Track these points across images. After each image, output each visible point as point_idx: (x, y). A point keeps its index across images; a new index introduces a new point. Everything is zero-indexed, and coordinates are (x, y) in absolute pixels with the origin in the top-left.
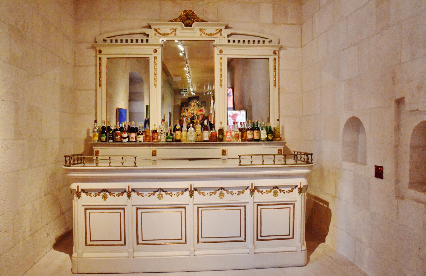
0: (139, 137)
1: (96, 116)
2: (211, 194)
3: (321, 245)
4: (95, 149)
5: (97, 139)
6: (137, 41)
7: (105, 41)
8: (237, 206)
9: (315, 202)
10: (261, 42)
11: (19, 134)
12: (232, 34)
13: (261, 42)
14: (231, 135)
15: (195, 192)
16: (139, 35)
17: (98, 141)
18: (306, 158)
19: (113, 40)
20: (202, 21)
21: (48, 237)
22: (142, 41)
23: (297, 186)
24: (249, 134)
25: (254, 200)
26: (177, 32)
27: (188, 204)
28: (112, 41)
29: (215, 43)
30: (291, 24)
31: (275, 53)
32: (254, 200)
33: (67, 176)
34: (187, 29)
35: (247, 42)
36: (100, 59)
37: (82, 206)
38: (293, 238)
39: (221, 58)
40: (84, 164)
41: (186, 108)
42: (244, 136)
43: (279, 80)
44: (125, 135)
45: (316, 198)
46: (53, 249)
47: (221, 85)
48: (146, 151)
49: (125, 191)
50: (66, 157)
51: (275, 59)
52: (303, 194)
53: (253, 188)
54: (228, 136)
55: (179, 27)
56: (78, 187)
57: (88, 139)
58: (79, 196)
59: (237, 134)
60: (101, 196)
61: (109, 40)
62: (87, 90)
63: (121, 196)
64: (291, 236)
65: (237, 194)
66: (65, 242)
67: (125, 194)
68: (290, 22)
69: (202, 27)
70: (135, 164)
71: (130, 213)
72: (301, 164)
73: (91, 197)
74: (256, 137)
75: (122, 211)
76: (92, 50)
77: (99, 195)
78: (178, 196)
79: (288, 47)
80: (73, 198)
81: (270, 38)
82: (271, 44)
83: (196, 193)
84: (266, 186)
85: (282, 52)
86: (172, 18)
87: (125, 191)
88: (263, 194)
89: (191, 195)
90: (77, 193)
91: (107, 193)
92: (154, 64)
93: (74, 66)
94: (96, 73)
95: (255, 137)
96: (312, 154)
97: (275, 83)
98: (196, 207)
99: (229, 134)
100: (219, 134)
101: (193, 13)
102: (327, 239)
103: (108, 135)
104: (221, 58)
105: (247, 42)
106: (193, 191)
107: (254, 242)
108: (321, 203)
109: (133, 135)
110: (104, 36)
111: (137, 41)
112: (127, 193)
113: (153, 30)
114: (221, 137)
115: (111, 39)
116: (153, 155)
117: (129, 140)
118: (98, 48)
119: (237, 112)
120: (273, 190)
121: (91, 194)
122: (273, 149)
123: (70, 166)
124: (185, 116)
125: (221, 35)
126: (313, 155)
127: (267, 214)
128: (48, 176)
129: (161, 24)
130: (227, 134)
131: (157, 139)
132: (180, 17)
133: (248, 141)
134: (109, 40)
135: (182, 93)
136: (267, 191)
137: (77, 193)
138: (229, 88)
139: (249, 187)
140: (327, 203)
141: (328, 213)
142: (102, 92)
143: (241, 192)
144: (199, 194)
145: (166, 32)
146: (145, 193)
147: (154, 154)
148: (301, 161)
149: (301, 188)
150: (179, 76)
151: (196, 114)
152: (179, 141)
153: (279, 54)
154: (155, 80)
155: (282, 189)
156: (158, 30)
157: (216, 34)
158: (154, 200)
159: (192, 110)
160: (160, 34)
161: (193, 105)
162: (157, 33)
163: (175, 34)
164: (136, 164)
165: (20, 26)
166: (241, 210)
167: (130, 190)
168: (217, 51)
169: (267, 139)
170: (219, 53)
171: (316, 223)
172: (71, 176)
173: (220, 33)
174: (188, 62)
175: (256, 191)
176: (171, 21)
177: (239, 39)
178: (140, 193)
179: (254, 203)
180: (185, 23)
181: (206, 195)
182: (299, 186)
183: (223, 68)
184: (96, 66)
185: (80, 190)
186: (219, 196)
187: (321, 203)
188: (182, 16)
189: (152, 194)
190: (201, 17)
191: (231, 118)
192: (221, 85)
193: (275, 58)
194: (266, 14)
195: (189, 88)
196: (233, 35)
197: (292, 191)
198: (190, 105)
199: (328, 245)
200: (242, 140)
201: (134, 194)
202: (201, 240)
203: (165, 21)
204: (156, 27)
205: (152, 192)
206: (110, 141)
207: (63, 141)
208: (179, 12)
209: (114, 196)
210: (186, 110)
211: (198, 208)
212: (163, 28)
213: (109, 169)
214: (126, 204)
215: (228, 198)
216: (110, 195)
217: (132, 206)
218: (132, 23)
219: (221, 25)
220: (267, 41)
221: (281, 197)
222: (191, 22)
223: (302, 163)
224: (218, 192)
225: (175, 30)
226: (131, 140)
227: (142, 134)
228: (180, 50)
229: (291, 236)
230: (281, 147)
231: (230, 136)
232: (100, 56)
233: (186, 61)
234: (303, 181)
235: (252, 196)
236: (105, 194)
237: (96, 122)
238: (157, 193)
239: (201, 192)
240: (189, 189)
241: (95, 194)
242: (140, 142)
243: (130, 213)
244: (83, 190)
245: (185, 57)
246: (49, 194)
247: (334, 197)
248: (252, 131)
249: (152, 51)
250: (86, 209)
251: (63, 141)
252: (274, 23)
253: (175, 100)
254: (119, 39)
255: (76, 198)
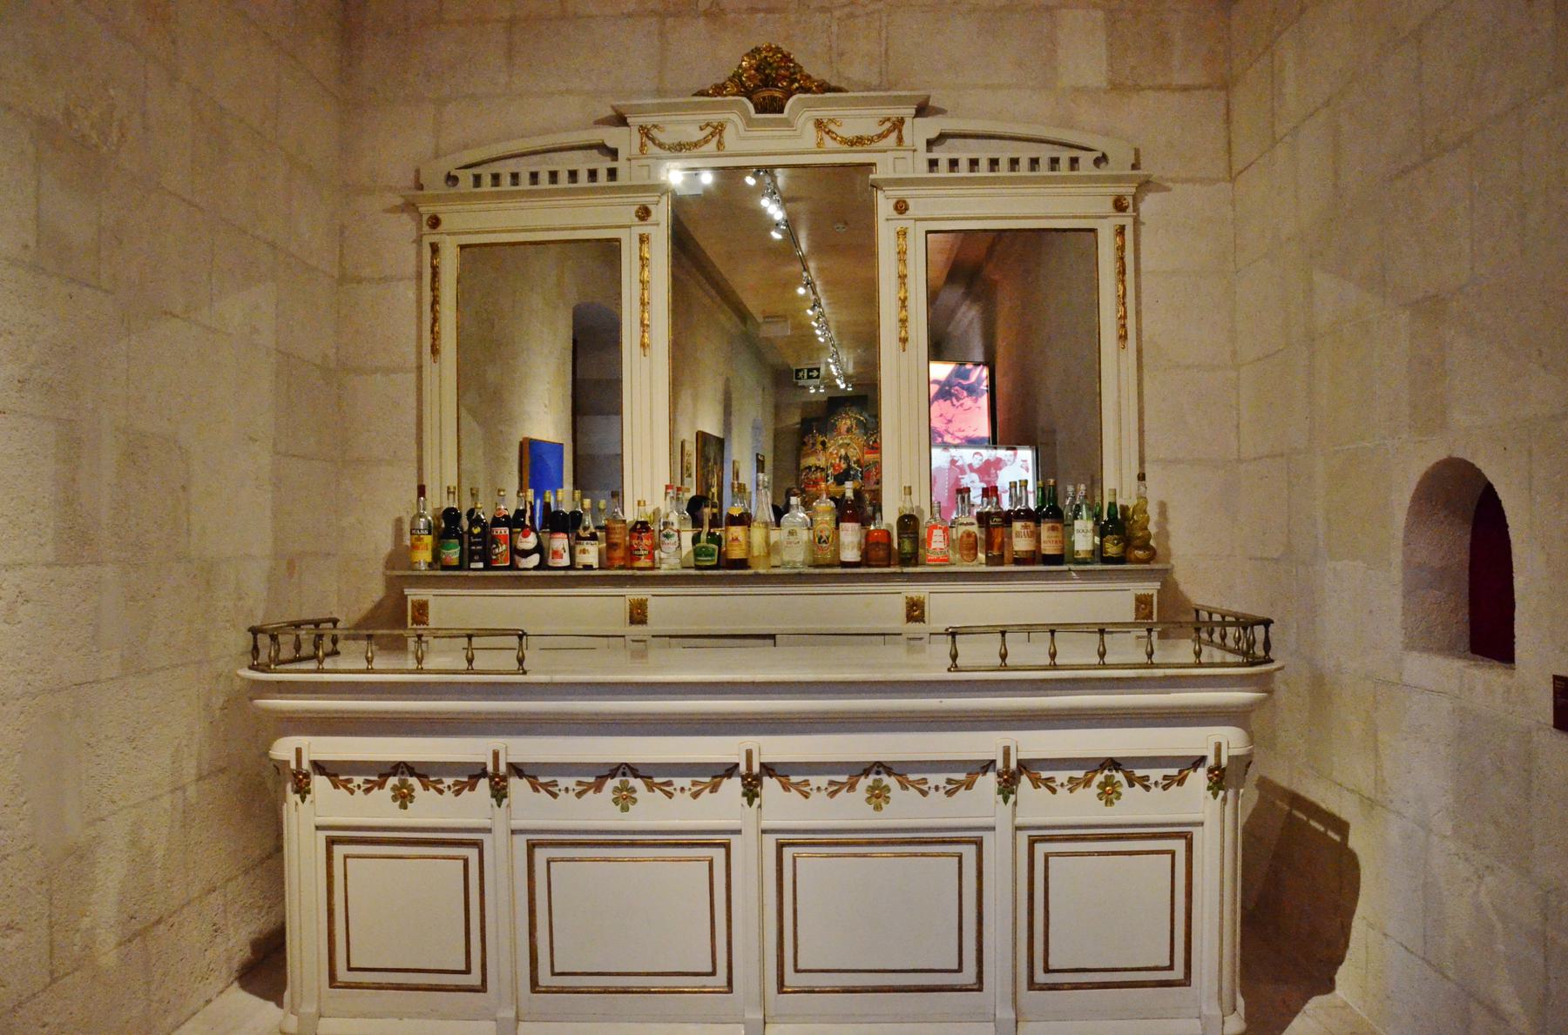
0: (584, 551)
1: (420, 469)
2: (834, 790)
3: (1315, 1002)
4: (414, 594)
5: (424, 556)
6: (573, 175)
7: (452, 179)
8: (943, 842)
9: (1290, 814)
10: (1064, 163)
11: (76, 541)
12: (943, 137)
13: (1064, 163)
14: (949, 541)
15: (766, 780)
16: (579, 153)
17: (430, 565)
18: (1250, 639)
19: (483, 178)
20: (825, 88)
21: (218, 940)
22: (593, 175)
23: (1203, 759)
24: (1018, 535)
25: (1014, 815)
26: (729, 134)
27: (738, 832)
28: (477, 180)
29: (878, 175)
30: (1185, 89)
31: (1119, 205)
32: (1014, 815)
33: (257, 708)
34: (766, 123)
35: (1004, 164)
36: (435, 249)
37: (318, 828)
38: (1186, 981)
39: (903, 234)
40: (321, 662)
41: (821, 439)
42: (999, 541)
43: (1138, 313)
44: (530, 542)
45: (1296, 800)
46: (236, 984)
47: (904, 340)
48: (605, 607)
49: (484, 774)
50: (255, 631)
51: (1121, 231)
52: (1231, 793)
53: (1013, 765)
54: (934, 546)
55: (736, 115)
56: (299, 751)
57: (399, 558)
58: (303, 790)
59: (969, 535)
60: (387, 792)
61: (466, 178)
62: (387, 371)
63: (466, 791)
64: (1178, 973)
65: (942, 791)
66: (265, 968)
67: (484, 784)
68: (1179, 79)
69: (824, 113)
70: (521, 661)
71: (504, 861)
72: (1224, 665)
73: (352, 792)
74: (1049, 548)
75: (472, 854)
76: (405, 217)
77: (381, 785)
78: (695, 795)
79: (1172, 180)
80: (284, 799)
81: (1101, 145)
82: (1104, 171)
83: (770, 785)
84: (1052, 760)
85: (1150, 204)
86: (708, 85)
87: (484, 774)
88: (1053, 791)
89: (751, 791)
90: (295, 776)
91: (413, 781)
92: (637, 263)
93: (343, 279)
94: (419, 301)
95: (1043, 546)
96: (1267, 623)
97: (1124, 326)
98: (770, 842)
99: (938, 534)
100: (899, 537)
101: (787, 58)
102: (1342, 975)
103: (468, 544)
104: (903, 234)
105: (1004, 164)
106: (758, 779)
107: (1015, 993)
108: (1313, 823)
109: (560, 542)
110: (448, 164)
111: (573, 175)
112: (491, 779)
113: (635, 130)
114: (907, 547)
115: (476, 171)
116: (632, 622)
117: (542, 565)
118: (426, 210)
119: (1002, 453)
120: (1099, 778)
121: (349, 781)
122: (1114, 599)
123: (265, 669)
124: (818, 468)
125: (900, 140)
126: (1272, 628)
127: (1074, 879)
128: (218, 701)
129: (662, 109)
130: (930, 535)
131: (651, 556)
132: (737, 76)
133: (1017, 562)
134: (466, 178)
135: (801, 383)
136: (1071, 780)
137: (295, 776)
138: (977, 364)
139: (993, 762)
140: (1342, 827)
141: (1348, 866)
142: (444, 374)
143: (960, 784)
144: (786, 787)
145: (684, 140)
146: (564, 782)
147: (638, 615)
148: (1223, 647)
149: (1218, 766)
150: (784, 318)
151: (858, 462)
152: (742, 564)
153: (1136, 209)
154: (642, 324)
155: (1139, 773)
156: (654, 132)
157: (882, 136)
158: (599, 811)
159: (841, 446)
160: (661, 145)
161: (844, 429)
162: (649, 143)
163: (720, 144)
164: (526, 665)
165: (87, 123)
166: (960, 857)
167: (503, 769)
168: (884, 205)
169: (1099, 555)
170: (895, 214)
171: (1293, 901)
172: (282, 712)
173: (894, 135)
174: (812, 265)
175: (1024, 779)
176: (702, 93)
177: (974, 156)
178: (542, 780)
179: (1018, 828)
180: (755, 97)
181: (814, 794)
182: (1211, 761)
183: (910, 272)
184: (419, 276)
185: (306, 766)
186: (868, 800)
187: (1313, 823)
188: (745, 70)
189: (589, 786)
190: (816, 70)
191: (975, 477)
192: (904, 340)
193: (1123, 228)
194: (1084, 57)
195: (828, 364)
196: (949, 142)
197: (1181, 782)
198: (834, 428)
199: (1346, 1006)
200: (990, 561)
201: (517, 786)
202: (791, 979)
203: (679, 93)
204: (648, 120)
205: (591, 780)
206: (473, 565)
207: (291, 565)
208: (731, 55)
209: (441, 792)
210: (819, 447)
211: (780, 846)
212: (671, 122)
213: (413, 684)
214: (485, 823)
215: (906, 809)
216: (426, 788)
217: (513, 832)
218: (555, 110)
219: (899, 101)
220: (1086, 159)
221: (1135, 806)
222: (778, 94)
223: (1230, 658)
224: (865, 783)
225: (718, 130)
226: (551, 563)
227: (593, 537)
228: (770, 218)
229: (1178, 973)
230: (1151, 588)
231: (942, 546)
232: (435, 239)
233: (803, 261)
234: (1231, 740)
235: (1006, 800)
236: (403, 784)
237: (421, 491)
238: (611, 784)
239: (794, 779)
240: (743, 769)
241: (367, 781)
242: (589, 567)
243: (504, 861)
244: (319, 767)
245: (797, 244)
246: (222, 770)
247: (1370, 804)
248: (1031, 524)
249: (629, 215)
250: (331, 842)
251: (289, 565)
252: (1115, 87)
253: (778, 411)
254: (505, 169)
255: (293, 798)
